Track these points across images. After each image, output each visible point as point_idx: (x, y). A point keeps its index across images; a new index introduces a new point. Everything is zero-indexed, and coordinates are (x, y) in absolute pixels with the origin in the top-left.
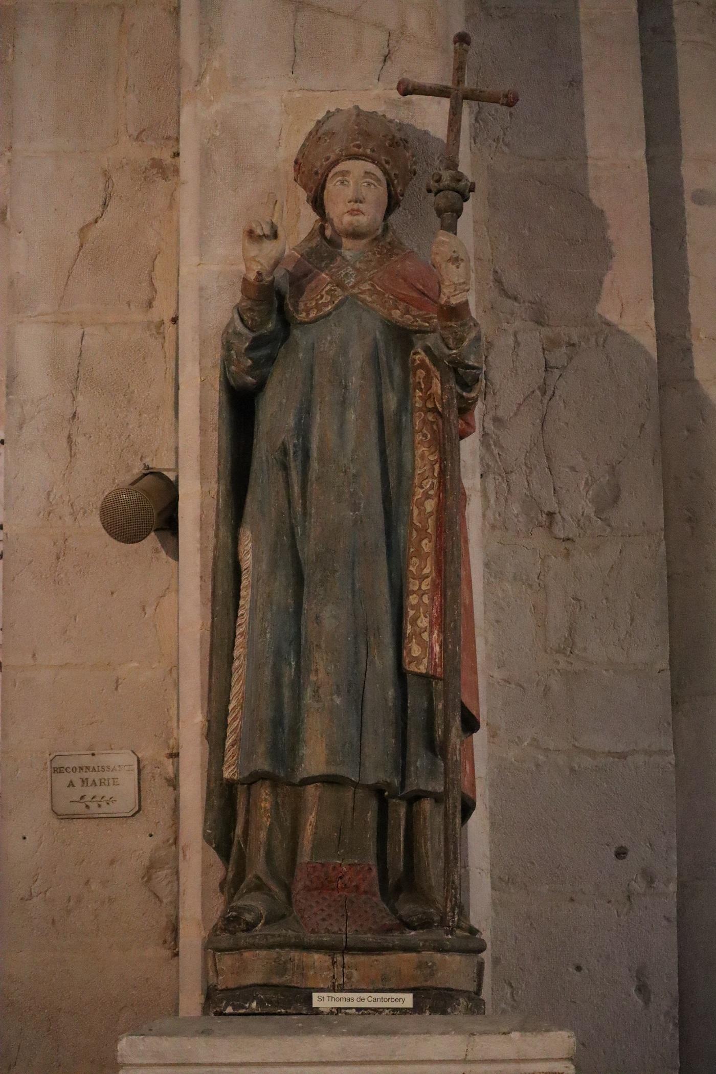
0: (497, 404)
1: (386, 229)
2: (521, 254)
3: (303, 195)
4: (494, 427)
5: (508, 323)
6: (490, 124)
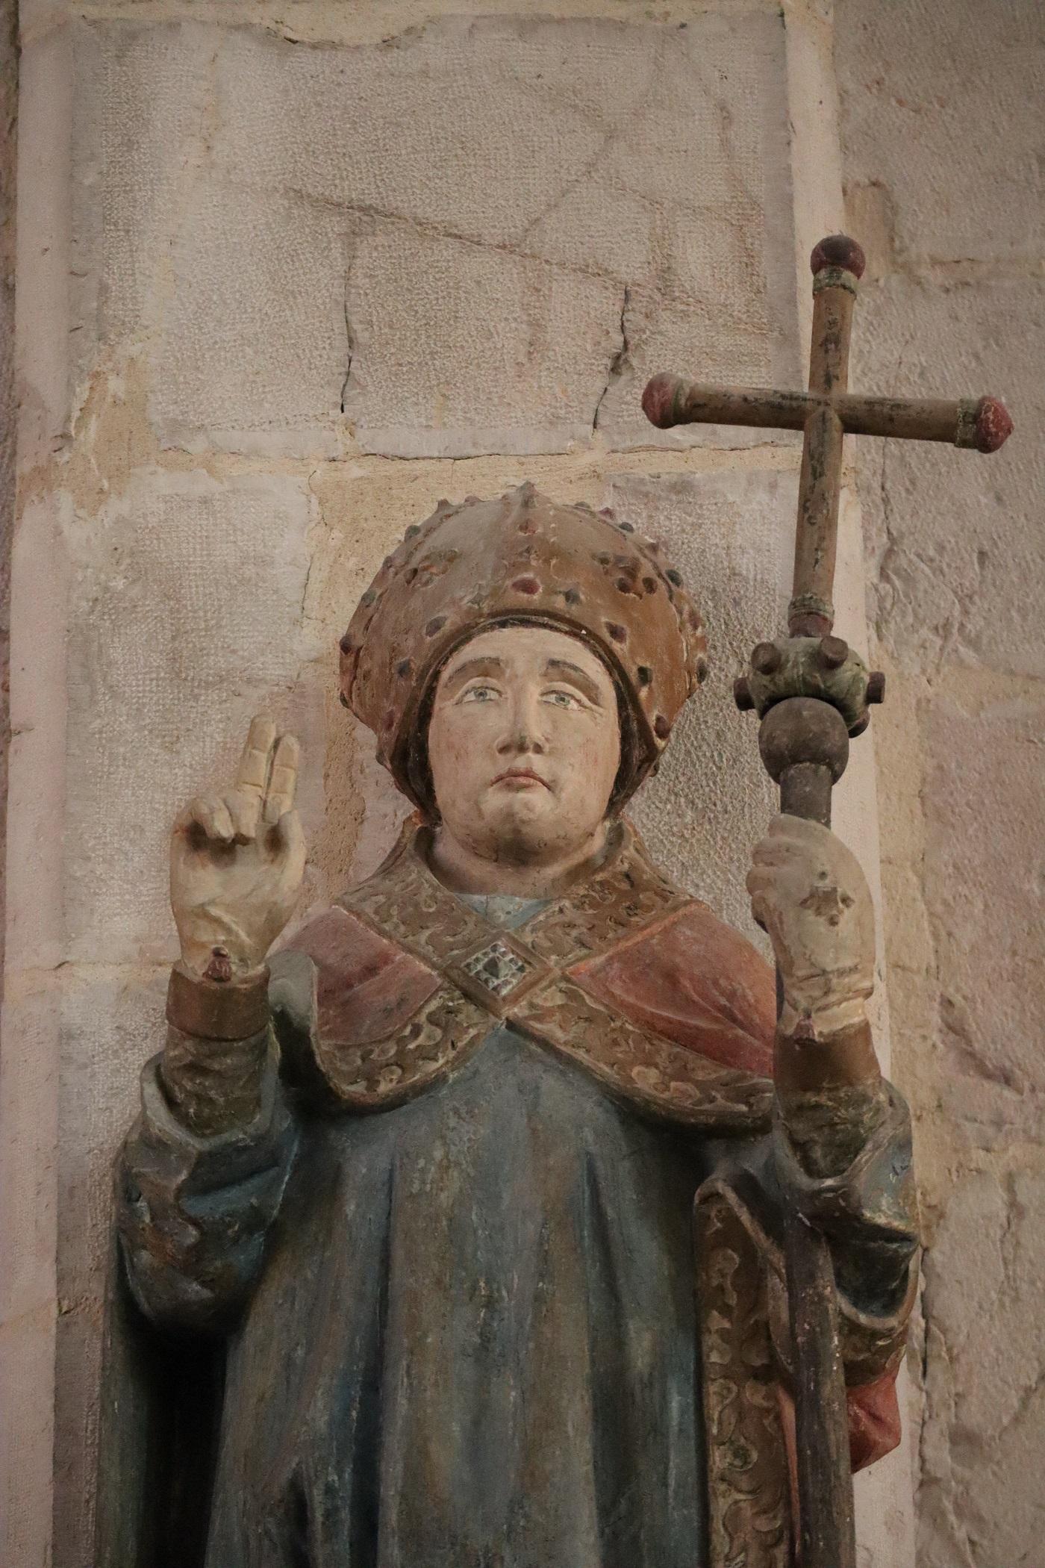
0: (960, 1389)
1: (617, 837)
2: (1020, 952)
3: (367, 739)
4: (955, 1456)
5: (988, 1150)
6: (923, 585)
